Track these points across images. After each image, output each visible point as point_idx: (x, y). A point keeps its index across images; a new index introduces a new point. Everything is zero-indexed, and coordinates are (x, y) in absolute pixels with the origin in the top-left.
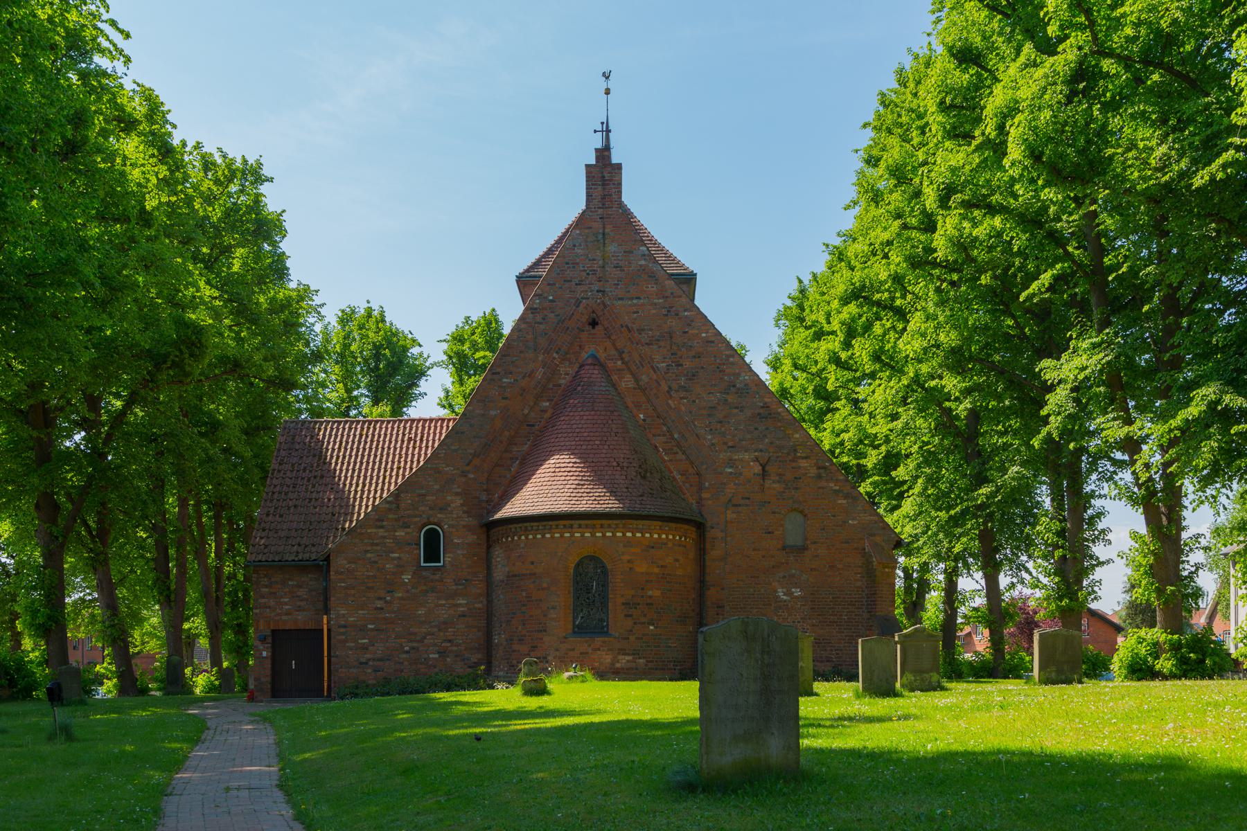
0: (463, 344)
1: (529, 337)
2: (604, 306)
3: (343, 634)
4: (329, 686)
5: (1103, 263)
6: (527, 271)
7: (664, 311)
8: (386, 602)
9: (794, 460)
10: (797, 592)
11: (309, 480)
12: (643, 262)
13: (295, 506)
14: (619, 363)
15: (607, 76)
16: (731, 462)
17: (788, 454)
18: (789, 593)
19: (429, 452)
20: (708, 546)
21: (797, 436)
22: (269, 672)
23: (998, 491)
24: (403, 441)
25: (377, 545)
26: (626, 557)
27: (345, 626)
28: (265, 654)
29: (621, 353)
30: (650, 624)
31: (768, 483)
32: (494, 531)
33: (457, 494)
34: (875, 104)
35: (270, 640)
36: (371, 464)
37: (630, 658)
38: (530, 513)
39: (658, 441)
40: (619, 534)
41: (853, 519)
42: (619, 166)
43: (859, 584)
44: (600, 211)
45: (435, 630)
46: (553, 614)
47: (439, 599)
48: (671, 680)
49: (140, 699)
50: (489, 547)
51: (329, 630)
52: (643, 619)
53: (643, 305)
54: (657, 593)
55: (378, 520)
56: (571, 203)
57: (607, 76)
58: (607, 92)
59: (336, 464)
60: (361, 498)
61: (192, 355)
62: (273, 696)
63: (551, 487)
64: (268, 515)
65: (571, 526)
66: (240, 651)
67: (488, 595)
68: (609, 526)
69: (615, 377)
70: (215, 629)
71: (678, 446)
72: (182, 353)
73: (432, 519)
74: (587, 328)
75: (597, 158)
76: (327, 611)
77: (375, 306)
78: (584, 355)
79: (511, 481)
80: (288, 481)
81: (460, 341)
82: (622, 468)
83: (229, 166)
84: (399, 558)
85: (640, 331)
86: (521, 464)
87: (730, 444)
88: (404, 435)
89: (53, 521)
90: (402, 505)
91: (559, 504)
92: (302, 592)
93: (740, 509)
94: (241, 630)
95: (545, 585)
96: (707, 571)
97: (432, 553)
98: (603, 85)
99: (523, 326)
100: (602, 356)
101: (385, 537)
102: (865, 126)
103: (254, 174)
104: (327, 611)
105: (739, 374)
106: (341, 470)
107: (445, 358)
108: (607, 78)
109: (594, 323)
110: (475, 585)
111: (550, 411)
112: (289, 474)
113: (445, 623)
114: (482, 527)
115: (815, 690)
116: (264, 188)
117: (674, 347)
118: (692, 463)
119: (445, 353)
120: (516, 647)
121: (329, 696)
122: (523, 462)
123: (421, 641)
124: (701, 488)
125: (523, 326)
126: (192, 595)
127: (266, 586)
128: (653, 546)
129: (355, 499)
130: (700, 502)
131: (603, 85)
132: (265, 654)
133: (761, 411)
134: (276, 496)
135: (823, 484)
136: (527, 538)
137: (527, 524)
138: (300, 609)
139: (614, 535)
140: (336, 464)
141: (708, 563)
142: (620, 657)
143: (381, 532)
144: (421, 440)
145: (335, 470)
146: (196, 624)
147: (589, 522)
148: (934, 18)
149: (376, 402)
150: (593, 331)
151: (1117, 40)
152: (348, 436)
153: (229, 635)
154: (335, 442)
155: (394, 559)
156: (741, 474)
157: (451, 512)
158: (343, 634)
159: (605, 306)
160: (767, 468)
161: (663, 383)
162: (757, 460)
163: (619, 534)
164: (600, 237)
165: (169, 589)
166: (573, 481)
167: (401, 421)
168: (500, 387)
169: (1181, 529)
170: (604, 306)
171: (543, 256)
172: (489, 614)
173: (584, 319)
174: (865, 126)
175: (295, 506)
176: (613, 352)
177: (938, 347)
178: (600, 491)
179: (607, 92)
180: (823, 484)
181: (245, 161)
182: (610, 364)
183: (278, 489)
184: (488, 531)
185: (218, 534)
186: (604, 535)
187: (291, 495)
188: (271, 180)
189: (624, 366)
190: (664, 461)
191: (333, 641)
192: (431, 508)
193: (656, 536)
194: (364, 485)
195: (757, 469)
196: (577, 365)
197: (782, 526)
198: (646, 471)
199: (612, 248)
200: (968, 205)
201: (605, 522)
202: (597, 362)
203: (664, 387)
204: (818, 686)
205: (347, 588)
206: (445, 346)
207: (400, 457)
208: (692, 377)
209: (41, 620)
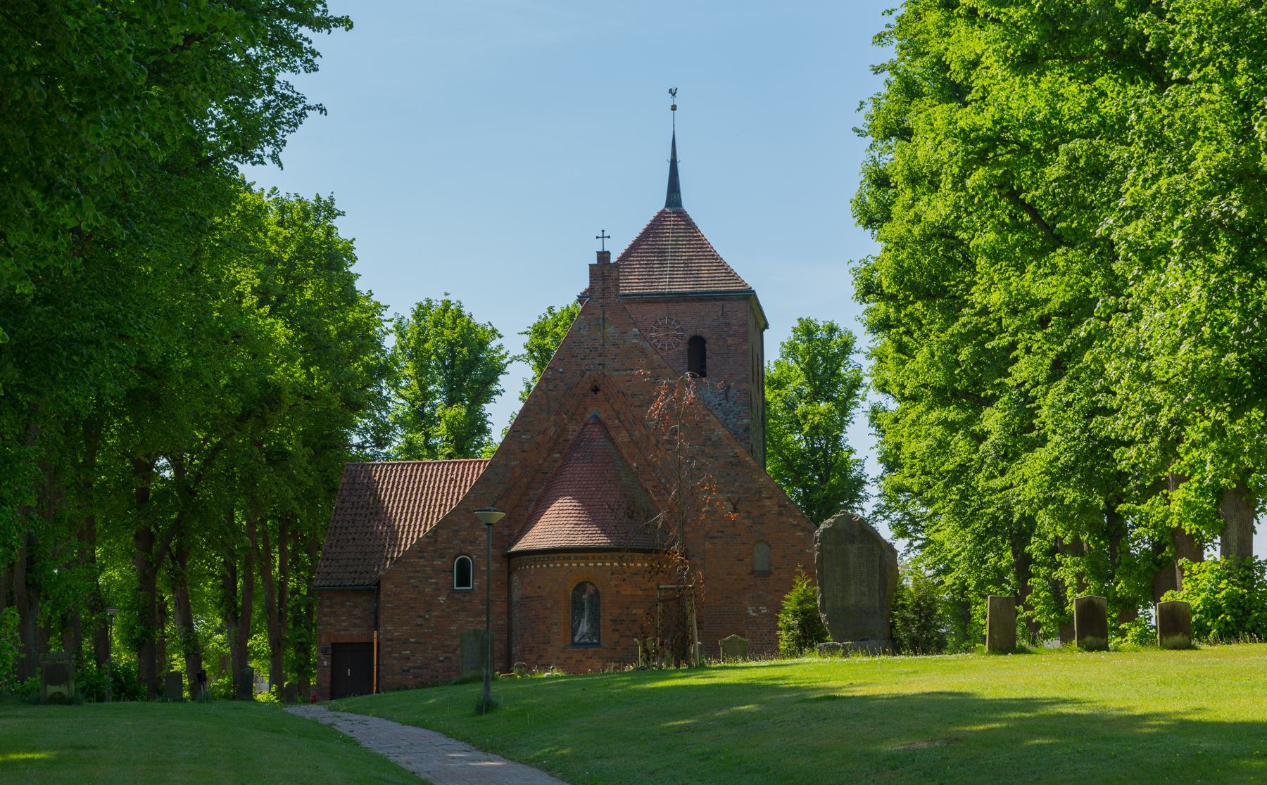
0: (544, 338)
2: (663, 320)
15: (673, 93)
18: (757, 611)
19: (434, 523)
22: (328, 678)
26: (613, 583)
32: (515, 561)
36: (421, 499)
38: (541, 547)
39: (648, 485)
50: (510, 573)
52: (628, 633)
54: (641, 612)
57: (673, 93)
58: (674, 108)
61: (271, 410)
63: (557, 527)
65: (569, 558)
66: (302, 669)
67: (509, 613)
69: (613, 433)
70: (277, 644)
75: (599, 259)
76: (377, 627)
80: (348, 518)
81: (542, 333)
83: (304, 209)
85: (633, 395)
89: (148, 550)
90: (439, 539)
91: (561, 542)
92: (357, 612)
94: (303, 649)
97: (463, 579)
100: (602, 416)
103: (327, 209)
104: (377, 627)
107: (525, 352)
109: (596, 390)
110: (485, 610)
116: (336, 222)
119: (526, 346)
126: (257, 610)
135: (784, 519)
138: (355, 625)
143: (422, 562)
146: (259, 641)
149: (450, 403)
153: (291, 653)
162: (729, 500)
165: (235, 605)
166: (572, 521)
170: (663, 320)
173: (588, 386)
178: (594, 528)
179: (674, 108)
180: (784, 519)
181: (319, 199)
182: (609, 423)
185: (282, 549)
187: (351, 530)
188: (343, 214)
199: (610, 330)
202: (598, 422)
209: (136, 636)
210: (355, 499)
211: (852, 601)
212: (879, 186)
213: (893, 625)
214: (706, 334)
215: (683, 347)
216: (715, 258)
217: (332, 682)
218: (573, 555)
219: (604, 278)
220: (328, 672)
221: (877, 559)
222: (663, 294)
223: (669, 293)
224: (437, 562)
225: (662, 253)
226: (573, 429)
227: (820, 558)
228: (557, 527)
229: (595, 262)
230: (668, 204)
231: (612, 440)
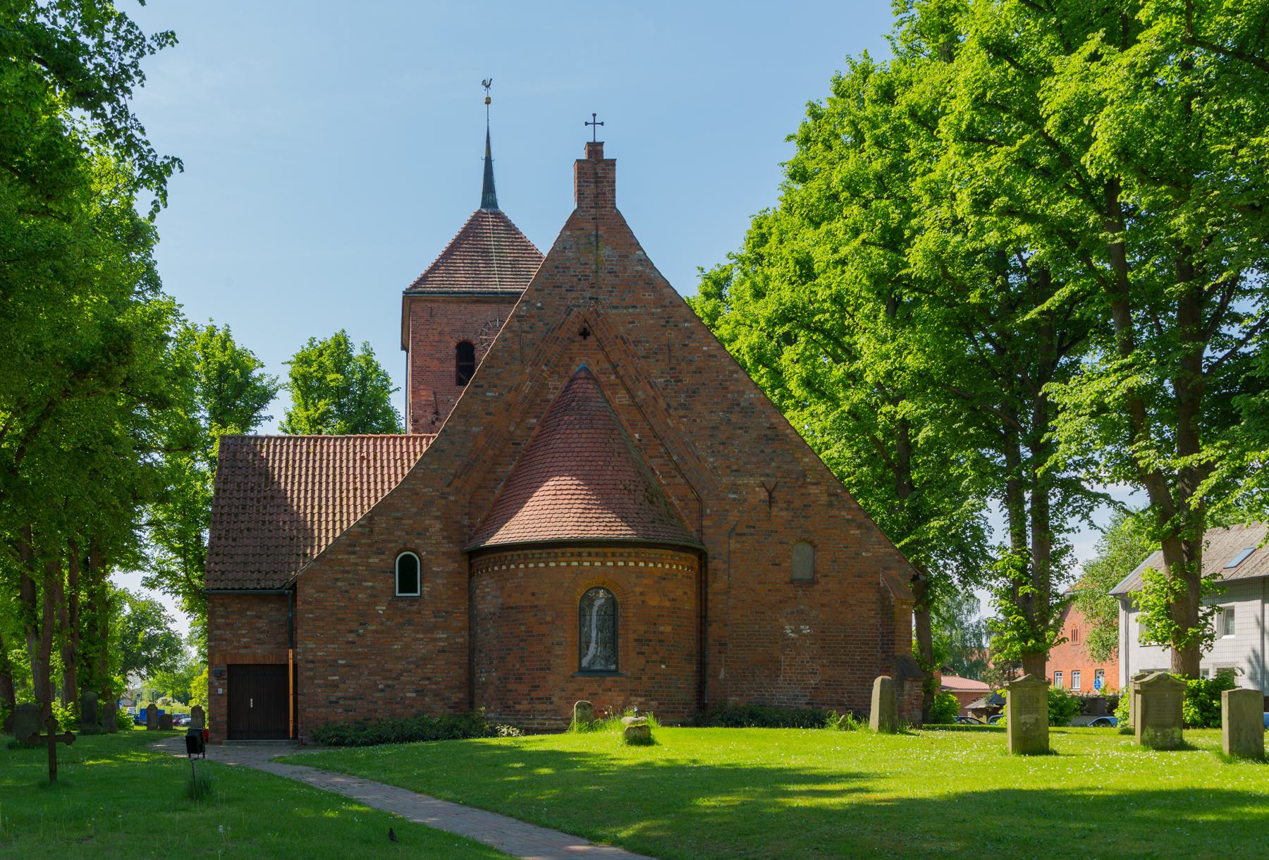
1: (516, 347)
3: (311, 670)
4: (295, 727)
5: (1127, 279)
6: (414, 286)
7: (662, 322)
8: (359, 635)
9: (804, 485)
10: (806, 630)
11: (258, 501)
12: (639, 268)
13: (248, 529)
14: (613, 377)
15: (487, 85)
16: (734, 487)
17: (797, 479)
20: (710, 578)
21: (807, 460)
22: (224, 711)
23: (952, 524)
24: (355, 460)
25: (348, 572)
26: (638, 590)
27: (313, 662)
28: (220, 691)
29: (615, 367)
30: (662, 662)
31: (775, 511)
32: (477, 558)
33: (436, 518)
34: (803, 115)
38: (533, 539)
39: (654, 463)
41: (867, 551)
42: (612, 163)
43: (872, 621)
44: (593, 211)
45: (413, 666)
46: (558, 651)
47: (417, 632)
48: (683, 725)
50: (471, 575)
51: (295, 666)
52: (655, 657)
53: (639, 314)
54: (669, 629)
55: (349, 545)
57: (487, 85)
58: (488, 101)
59: (286, 484)
60: (320, 521)
61: (119, 363)
62: (229, 738)
63: (550, 512)
64: (219, 538)
65: (580, 554)
68: (621, 555)
69: (608, 393)
71: (677, 468)
72: (109, 360)
73: (409, 545)
74: (579, 338)
75: (590, 153)
77: (221, 326)
79: (495, 505)
80: (237, 503)
82: (630, 491)
84: (372, 587)
85: (637, 343)
86: (506, 486)
87: (734, 467)
88: (355, 454)
92: (261, 624)
93: (744, 538)
95: (549, 619)
96: (710, 605)
97: (408, 583)
98: (492, 93)
99: (508, 335)
100: (594, 370)
101: (357, 564)
102: (790, 138)
104: (294, 646)
105: (743, 392)
106: (292, 491)
107: (290, 380)
108: (488, 86)
109: (585, 334)
111: (538, 429)
112: (235, 494)
113: (423, 659)
114: (463, 553)
115: (1053, 745)
118: (692, 487)
119: (291, 375)
120: (512, 686)
121: (295, 736)
122: (509, 482)
123: (397, 678)
124: (701, 515)
125: (508, 335)
127: (222, 617)
129: (312, 522)
130: (700, 530)
131: (492, 93)
132: (220, 691)
133: (768, 432)
134: (225, 518)
135: (835, 512)
136: (526, 567)
137: (528, 552)
138: (260, 642)
140: (286, 484)
141: (710, 597)
144: (375, 459)
145: (286, 490)
147: (600, 550)
148: (897, 19)
150: (584, 342)
151: (1210, 29)
152: (295, 454)
154: (281, 461)
155: (367, 588)
156: (745, 500)
157: (430, 538)
158: (311, 670)
160: (774, 494)
161: (661, 401)
162: (763, 485)
163: (632, 564)
164: (593, 239)
166: (578, 505)
167: (395, 438)
168: (484, 401)
169: (1200, 567)
171: (429, 272)
172: (472, 650)
174: (790, 138)
175: (248, 529)
176: (607, 365)
177: (903, 369)
178: (609, 516)
179: (488, 101)
180: (835, 512)
182: (603, 379)
183: (226, 510)
184: (470, 558)
186: (615, 564)
187: (241, 518)
189: (618, 381)
190: (661, 485)
191: (300, 678)
192: (407, 533)
193: (632, 564)
194: (320, 508)
195: (763, 495)
196: (567, 379)
197: (790, 557)
199: (605, 251)
200: (1008, 212)
202: (590, 377)
203: (662, 404)
205: (314, 620)
206: (289, 368)
207: (355, 478)
208: (693, 393)
210: (240, 479)
215: (453, 351)
217: (229, 715)
218: (585, 551)
219: (598, 180)
222: (496, 293)
223: (502, 293)
224: (374, 560)
225: (485, 253)
228: (550, 512)
229: (584, 156)
230: (484, 205)
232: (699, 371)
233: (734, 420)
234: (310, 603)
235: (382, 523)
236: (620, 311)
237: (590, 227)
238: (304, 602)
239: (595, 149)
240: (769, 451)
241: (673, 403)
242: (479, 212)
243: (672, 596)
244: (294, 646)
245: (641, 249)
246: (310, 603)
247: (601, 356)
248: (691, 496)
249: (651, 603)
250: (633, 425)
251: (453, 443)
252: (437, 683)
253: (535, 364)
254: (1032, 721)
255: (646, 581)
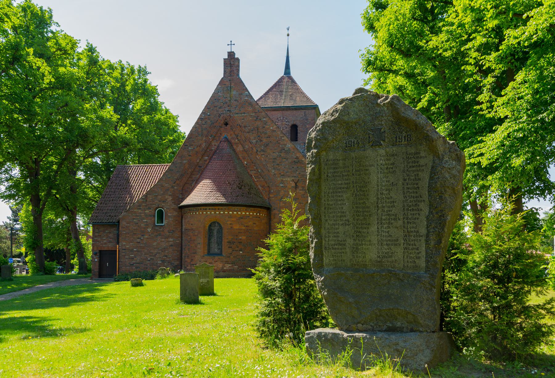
3: (123, 252)
16: (282, 182)
20: (272, 217)
22: (97, 267)
26: (229, 223)
28: (96, 260)
30: (240, 251)
33: (170, 195)
35: (98, 254)
37: (230, 265)
38: (190, 203)
39: (252, 173)
40: (226, 213)
44: (229, 78)
46: (199, 246)
47: (162, 238)
49: (48, 276)
52: (237, 249)
56: (218, 73)
58: (288, 35)
65: (206, 209)
68: (222, 209)
69: (235, 147)
74: (224, 126)
78: (222, 137)
80: (113, 190)
82: (230, 184)
85: (245, 127)
90: (148, 200)
92: (111, 235)
97: (161, 219)
100: (229, 138)
103: (143, 72)
104: (118, 243)
105: (286, 145)
109: (226, 124)
113: (164, 248)
116: (148, 77)
117: (259, 133)
118: (266, 182)
124: (270, 193)
127: (97, 233)
128: (242, 217)
131: (290, 32)
132: (96, 260)
133: (295, 160)
138: (110, 242)
139: (224, 213)
142: (226, 265)
147: (213, 207)
159: (231, 117)
161: (254, 149)
162: (293, 180)
163: (226, 213)
176: (234, 136)
179: (288, 35)
182: (233, 141)
186: (220, 213)
191: (120, 255)
198: (242, 186)
199: (234, 93)
201: (220, 207)
202: (227, 140)
204: (219, 284)
205: (126, 234)
208: (267, 145)
211: (372, 254)
212: (377, 9)
213: (445, 296)
214: (298, 123)
215: (289, 129)
216: (302, 93)
219: (231, 66)
220: (98, 264)
221: (425, 176)
225: (281, 92)
226: (215, 144)
227: (317, 177)
228: (202, 193)
229: (227, 57)
230: (285, 74)
231: (234, 150)
232: (269, 137)
233: (282, 155)
234: (124, 228)
235: (150, 198)
236: (239, 115)
237: (228, 84)
238: (123, 228)
239: (231, 55)
240: (295, 167)
241: (259, 150)
242: (283, 76)
243: (246, 225)
244: (118, 244)
245: (247, 91)
246: (124, 228)
247: (232, 132)
248: (266, 185)
249: (235, 228)
250: (244, 158)
251: (176, 167)
252: (169, 258)
253: (207, 136)
254: (206, 281)
255: (232, 219)
